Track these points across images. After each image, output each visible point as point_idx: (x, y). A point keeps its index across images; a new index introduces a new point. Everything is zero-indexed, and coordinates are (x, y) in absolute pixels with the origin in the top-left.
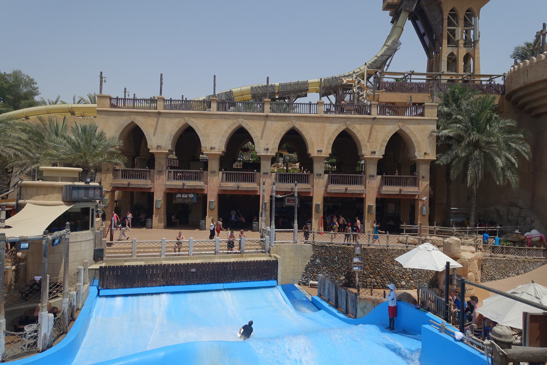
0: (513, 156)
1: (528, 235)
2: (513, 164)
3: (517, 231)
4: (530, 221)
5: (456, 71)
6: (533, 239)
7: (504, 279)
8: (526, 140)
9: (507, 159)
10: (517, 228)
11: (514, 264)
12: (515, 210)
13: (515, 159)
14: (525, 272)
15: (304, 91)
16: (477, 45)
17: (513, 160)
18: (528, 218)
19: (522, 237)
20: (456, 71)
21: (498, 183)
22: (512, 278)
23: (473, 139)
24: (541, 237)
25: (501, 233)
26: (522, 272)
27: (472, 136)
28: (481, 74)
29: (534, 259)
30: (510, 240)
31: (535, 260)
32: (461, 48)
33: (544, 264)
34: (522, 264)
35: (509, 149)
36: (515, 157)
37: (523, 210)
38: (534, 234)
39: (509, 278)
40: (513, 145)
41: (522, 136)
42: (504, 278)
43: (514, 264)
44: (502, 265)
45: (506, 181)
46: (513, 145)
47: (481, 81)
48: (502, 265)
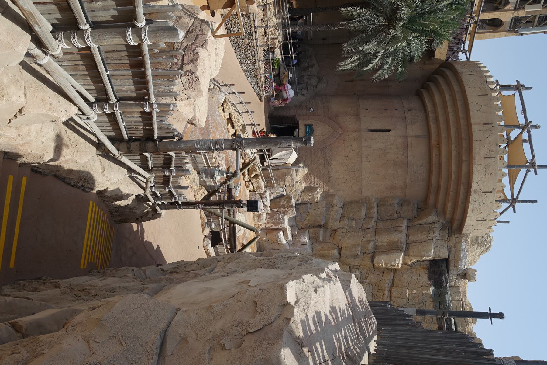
0: (376, 64)
1: (288, 87)
2: (366, 64)
3: (291, 75)
4: (303, 93)
5: (483, 11)
6: (284, 92)
7: (231, 46)
8: (395, 73)
9: (375, 54)
10: (294, 75)
11: (251, 57)
12: (314, 81)
13: (373, 67)
14: (244, 71)
15: (406, 27)
16: (510, 33)
17: (371, 65)
18: (306, 91)
19: (285, 82)
20: (483, 11)
21: (345, 45)
22: (235, 55)
23: (402, 10)
24: (287, 99)
25: (287, 60)
26: (244, 68)
27: (406, 10)
28: (475, 41)
29: (262, 85)
30: (281, 70)
31: (261, 86)
32: (513, 14)
33: (258, 95)
34: (252, 68)
35: (386, 56)
36: (375, 67)
37: (315, 88)
38: (290, 93)
39: (233, 52)
40: (390, 60)
41: (399, 71)
42: (232, 45)
43: (251, 57)
44: (247, 42)
45: (347, 56)
46: (390, 60)
47: (464, 43)
48: (247, 42)
